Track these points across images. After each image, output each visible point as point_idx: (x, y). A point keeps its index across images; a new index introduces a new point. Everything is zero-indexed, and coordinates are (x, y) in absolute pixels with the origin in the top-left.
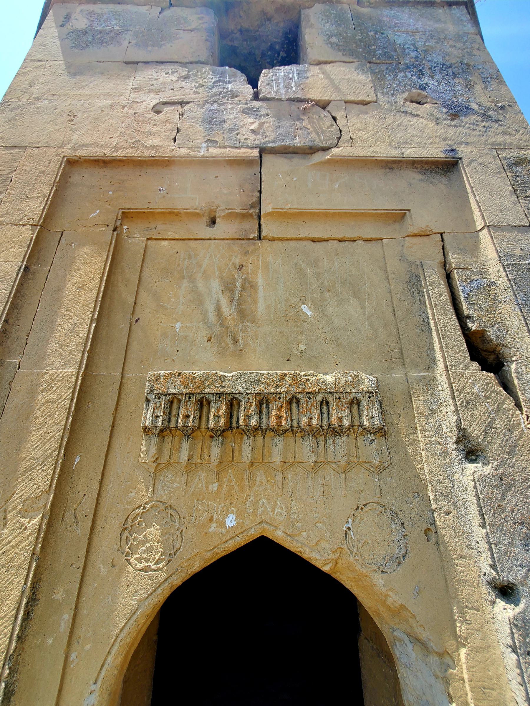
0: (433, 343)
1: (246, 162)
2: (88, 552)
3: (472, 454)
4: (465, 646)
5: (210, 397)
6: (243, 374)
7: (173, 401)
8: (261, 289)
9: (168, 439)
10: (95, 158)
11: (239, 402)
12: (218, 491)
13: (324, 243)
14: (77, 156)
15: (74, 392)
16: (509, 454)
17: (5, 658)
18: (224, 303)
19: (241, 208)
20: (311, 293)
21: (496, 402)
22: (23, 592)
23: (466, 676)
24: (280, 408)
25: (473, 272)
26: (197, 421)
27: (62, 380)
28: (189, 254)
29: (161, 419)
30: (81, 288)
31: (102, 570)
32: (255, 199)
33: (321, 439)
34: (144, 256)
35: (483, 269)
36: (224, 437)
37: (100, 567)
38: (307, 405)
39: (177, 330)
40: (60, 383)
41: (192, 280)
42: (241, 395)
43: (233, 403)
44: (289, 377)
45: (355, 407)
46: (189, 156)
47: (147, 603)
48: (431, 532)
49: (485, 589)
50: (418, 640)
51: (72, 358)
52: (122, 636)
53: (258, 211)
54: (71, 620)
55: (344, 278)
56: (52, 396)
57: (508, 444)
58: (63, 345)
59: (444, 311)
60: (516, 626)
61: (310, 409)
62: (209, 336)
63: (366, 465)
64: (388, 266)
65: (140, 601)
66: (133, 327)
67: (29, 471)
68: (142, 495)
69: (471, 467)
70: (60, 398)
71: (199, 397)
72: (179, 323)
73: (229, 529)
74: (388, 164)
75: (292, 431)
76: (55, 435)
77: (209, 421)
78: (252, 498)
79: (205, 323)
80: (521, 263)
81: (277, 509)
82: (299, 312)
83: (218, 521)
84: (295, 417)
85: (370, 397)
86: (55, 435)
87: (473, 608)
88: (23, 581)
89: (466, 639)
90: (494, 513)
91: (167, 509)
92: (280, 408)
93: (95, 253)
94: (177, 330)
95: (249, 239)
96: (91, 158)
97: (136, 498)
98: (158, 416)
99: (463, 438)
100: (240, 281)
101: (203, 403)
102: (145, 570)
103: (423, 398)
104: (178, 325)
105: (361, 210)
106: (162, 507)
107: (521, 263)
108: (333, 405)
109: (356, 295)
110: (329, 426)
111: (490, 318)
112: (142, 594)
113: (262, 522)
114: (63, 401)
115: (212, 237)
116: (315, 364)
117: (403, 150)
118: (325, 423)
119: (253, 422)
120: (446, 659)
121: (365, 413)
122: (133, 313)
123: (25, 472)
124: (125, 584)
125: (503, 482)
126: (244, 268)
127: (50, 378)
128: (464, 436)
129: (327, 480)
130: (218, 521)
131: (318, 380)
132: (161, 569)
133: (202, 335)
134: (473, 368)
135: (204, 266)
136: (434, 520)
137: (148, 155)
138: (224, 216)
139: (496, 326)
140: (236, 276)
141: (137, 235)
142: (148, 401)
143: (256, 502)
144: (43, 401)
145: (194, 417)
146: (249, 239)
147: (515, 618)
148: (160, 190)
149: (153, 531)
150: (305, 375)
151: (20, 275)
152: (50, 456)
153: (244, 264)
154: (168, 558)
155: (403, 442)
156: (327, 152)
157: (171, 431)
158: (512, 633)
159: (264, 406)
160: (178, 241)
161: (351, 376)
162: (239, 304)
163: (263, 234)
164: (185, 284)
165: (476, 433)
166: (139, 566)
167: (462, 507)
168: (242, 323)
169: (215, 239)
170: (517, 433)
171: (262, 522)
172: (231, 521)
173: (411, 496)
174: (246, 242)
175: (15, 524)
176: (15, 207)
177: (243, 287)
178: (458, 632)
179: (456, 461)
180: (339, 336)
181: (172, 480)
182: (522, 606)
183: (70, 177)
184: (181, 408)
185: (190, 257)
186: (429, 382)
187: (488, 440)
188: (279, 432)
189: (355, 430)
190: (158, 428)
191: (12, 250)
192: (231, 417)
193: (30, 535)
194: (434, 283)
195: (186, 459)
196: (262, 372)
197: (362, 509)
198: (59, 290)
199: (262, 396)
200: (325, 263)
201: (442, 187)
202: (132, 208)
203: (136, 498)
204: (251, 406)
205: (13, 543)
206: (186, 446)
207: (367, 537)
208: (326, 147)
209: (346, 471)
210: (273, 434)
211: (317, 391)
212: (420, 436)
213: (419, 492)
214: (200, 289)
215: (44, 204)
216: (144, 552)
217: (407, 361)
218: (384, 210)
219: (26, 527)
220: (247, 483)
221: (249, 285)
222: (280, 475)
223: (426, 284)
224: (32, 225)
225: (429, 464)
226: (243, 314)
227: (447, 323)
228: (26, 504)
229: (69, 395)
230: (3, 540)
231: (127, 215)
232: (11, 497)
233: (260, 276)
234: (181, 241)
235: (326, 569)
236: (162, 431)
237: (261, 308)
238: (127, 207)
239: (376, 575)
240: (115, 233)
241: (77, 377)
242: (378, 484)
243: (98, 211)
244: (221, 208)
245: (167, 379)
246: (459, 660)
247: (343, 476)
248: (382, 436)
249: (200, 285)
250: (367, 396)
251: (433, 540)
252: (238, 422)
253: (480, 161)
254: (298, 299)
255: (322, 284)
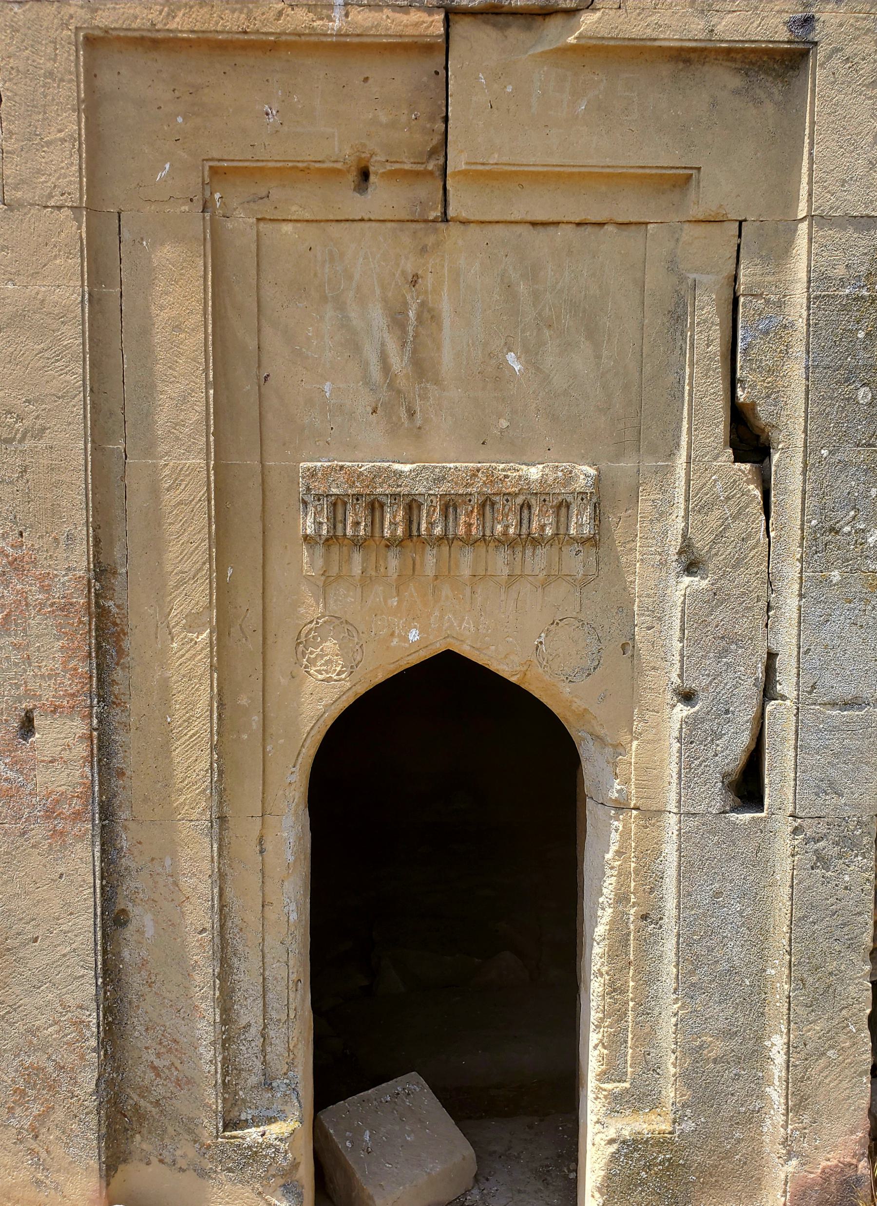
0: (681, 420)
1: (420, 48)
2: (264, 665)
3: (691, 567)
4: (637, 739)
5: (383, 499)
6: (424, 467)
7: (337, 504)
8: (446, 323)
9: (335, 549)
10: (137, 34)
11: (420, 505)
12: (399, 606)
13: (551, 230)
14: (101, 28)
15: (209, 489)
16: (733, 567)
17: (211, 747)
18: (392, 347)
19: (412, 160)
20: (523, 331)
21: (738, 504)
22: (211, 698)
23: (633, 761)
24: (469, 514)
25: (768, 301)
26: (369, 529)
27: (188, 475)
28: (331, 252)
29: (325, 527)
30: (178, 328)
31: (282, 680)
32: (437, 139)
33: (519, 549)
34: (258, 255)
35: (785, 296)
36: (402, 547)
37: (279, 678)
38: (503, 509)
39: (328, 394)
40: (188, 479)
41: (341, 307)
42: (422, 497)
43: (412, 506)
44: (483, 472)
45: (563, 510)
46: (313, 32)
47: (333, 707)
48: (627, 647)
49: (669, 695)
50: (598, 737)
51: (194, 443)
52: (313, 733)
53: (441, 161)
54: (261, 721)
55: (575, 302)
56: (183, 496)
57: (736, 556)
58: (176, 424)
59: (708, 370)
60: (686, 722)
61: (507, 515)
62: (374, 405)
63: (568, 578)
64: (647, 281)
65: (325, 706)
66: (262, 390)
67: (182, 585)
68: (311, 608)
69: (687, 580)
70: (193, 500)
71: (369, 499)
72: (328, 383)
73: (412, 642)
74: (683, 53)
75: (485, 540)
76: (200, 544)
77: (378, 527)
78: (437, 613)
79: (367, 384)
80: (836, 293)
81: (464, 624)
82: (502, 365)
83: (400, 636)
84: (488, 524)
85: (582, 499)
86: (200, 544)
87: (653, 711)
88: (209, 688)
89: (640, 734)
90: (696, 628)
91: (340, 624)
92: (469, 514)
93: (185, 261)
94: (328, 394)
95: (426, 221)
96: (129, 34)
97: (307, 613)
98: (321, 523)
99: (686, 547)
100: (414, 308)
101: (375, 506)
102: (328, 680)
103: (652, 497)
104: (327, 387)
105: (617, 167)
106: (337, 622)
107: (836, 293)
108: (536, 510)
109: (591, 334)
110: (529, 534)
111: (768, 383)
112: (327, 700)
113: (448, 637)
114: (197, 503)
115: (366, 218)
116: (518, 449)
117: (715, 20)
118: (524, 531)
119: (438, 531)
120: (619, 749)
121: (574, 519)
122: (259, 366)
123: (177, 587)
124: (308, 692)
125: (716, 597)
126: (420, 280)
127: (173, 472)
128: (688, 546)
129: (522, 594)
130: (400, 636)
131: (520, 476)
132: (343, 680)
133: (363, 402)
134: (724, 458)
135: (357, 277)
136: (634, 635)
137: (235, 28)
138: (384, 173)
139: (773, 396)
140: (408, 297)
141: (240, 214)
142: (305, 503)
143: (442, 617)
144: (173, 503)
145: (366, 525)
146: (426, 221)
147: (687, 717)
148: (267, 114)
149: (330, 645)
150: (503, 470)
151: (87, 310)
152: (200, 569)
153: (420, 273)
154: (349, 670)
155: (617, 552)
156: (573, 22)
157: (337, 539)
158: (681, 728)
159: (451, 509)
160: (310, 224)
161: (562, 471)
162: (415, 351)
163: (451, 213)
164: (330, 312)
165: (701, 543)
166: (320, 677)
167: (667, 623)
168: (420, 383)
169: (370, 220)
170: (752, 542)
171: (448, 637)
172: (414, 635)
173: (614, 611)
174: (422, 225)
175: (183, 639)
176: (29, 165)
177: (419, 317)
178: (634, 729)
179: (673, 574)
180: (556, 405)
181: (344, 594)
182: (697, 708)
183: (95, 76)
184: (347, 512)
185: (332, 259)
186: (669, 470)
187: (714, 551)
188: (469, 541)
189: (560, 538)
190: (323, 538)
191: (58, 262)
192: (411, 522)
193: (202, 649)
194: (705, 321)
195: (360, 572)
196: (448, 465)
197: (557, 624)
198: (146, 332)
199: (448, 498)
200: (550, 271)
201: (769, 108)
202: (225, 157)
203: (307, 613)
204: (434, 510)
205: (187, 656)
206: (357, 557)
207: (560, 650)
208: (570, 8)
209: (544, 585)
210: (461, 543)
211: (517, 492)
212: (638, 544)
213: (624, 608)
214: (354, 323)
215: (76, 156)
216: (323, 665)
217: (643, 444)
218: (657, 167)
219: (196, 643)
220: (430, 598)
221: (429, 315)
222: (468, 590)
223: (692, 323)
224: (71, 207)
225: (642, 577)
226: (422, 368)
227: (707, 391)
228: (188, 619)
229: (203, 495)
230: (176, 653)
231: (218, 174)
232: (170, 613)
233: (445, 297)
234: (314, 224)
235: (513, 679)
236: (327, 540)
237: (447, 360)
238: (216, 155)
239: (564, 684)
240: (207, 216)
241: (208, 471)
242: (578, 599)
243: (167, 166)
244: (378, 158)
245: (326, 475)
246: (631, 750)
247: (540, 590)
248: (593, 546)
249: (352, 315)
250: (580, 497)
251: (629, 653)
252: (419, 529)
253: (848, 51)
254: (503, 342)
255: (540, 314)
